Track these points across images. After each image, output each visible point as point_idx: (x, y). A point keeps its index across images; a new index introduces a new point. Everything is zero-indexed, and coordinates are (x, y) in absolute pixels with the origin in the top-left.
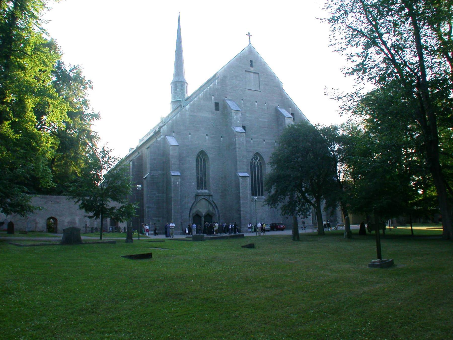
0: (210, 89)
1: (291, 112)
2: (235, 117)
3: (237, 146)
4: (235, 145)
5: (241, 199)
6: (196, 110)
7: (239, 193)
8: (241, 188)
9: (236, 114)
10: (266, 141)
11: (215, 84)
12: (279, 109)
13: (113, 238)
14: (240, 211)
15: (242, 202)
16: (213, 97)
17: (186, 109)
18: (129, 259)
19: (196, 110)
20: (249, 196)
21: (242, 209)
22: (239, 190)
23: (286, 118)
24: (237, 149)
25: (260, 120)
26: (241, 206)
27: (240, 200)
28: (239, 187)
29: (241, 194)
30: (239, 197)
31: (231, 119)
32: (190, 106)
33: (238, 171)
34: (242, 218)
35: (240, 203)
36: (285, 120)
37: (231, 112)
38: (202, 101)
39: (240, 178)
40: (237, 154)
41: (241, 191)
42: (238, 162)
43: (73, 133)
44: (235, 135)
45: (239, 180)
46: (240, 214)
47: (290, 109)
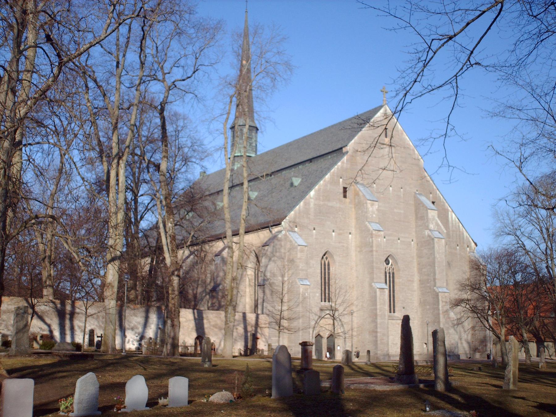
0: (338, 168)
1: (432, 200)
2: (371, 209)
3: (374, 249)
4: (372, 247)
5: (378, 318)
6: (321, 198)
7: (376, 309)
8: (378, 304)
9: (372, 205)
10: (401, 239)
11: (343, 163)
12: (418, 196)
13: (253, 360)
14: (376, 332)
15: (379, 321)
16: (341, 180)
17: (310, 196)
18: (57, 316)
19: (321, 198)
20: (386, 314)
21: (379, 330)
22: (376, 305)
23: (429, 211)
24: (374, 253)
25: (396, 211)
26: (379, 325)
27: (376, 318)
28: (376, 300)
29: (378, 311)
30: (376, 315)
31: (366, 212)
32: (315, 191)
33: (375, 281)
34: (379, 342)
35: (376, 323)
36: (427, 213)
37: (366, 203)
38: (329, 185)
39: (378, 290)
40: (374, 260)
41: (378, 307)
42: (375, 270)
43: (171, 216)
44: (372, 234)
45: (375, 292)
46: (376, 337)
47: (431, 195)
